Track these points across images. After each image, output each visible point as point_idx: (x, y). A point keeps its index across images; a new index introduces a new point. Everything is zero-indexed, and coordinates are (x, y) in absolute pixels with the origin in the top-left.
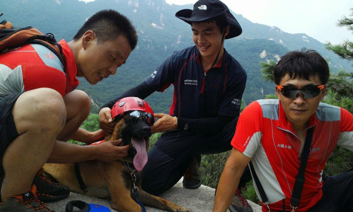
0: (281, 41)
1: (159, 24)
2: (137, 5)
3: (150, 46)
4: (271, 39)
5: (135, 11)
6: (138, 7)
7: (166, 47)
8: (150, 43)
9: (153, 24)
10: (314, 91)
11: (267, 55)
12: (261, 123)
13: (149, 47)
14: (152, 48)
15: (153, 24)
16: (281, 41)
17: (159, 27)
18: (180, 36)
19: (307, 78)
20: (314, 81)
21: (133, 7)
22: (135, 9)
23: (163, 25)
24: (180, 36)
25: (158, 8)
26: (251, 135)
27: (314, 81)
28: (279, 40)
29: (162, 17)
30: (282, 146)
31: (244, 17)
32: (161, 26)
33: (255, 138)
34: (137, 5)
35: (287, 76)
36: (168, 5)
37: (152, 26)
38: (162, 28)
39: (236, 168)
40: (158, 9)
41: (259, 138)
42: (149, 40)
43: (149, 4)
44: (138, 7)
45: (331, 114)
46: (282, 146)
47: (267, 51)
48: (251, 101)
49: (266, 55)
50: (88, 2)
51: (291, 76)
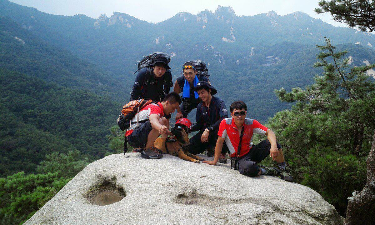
0: (369, 44)
1: (229, 38)
2: (206, 21)
3: (221, 61)
4: (358, 43)
5: (204, 27)
6: (207, 22)
7: (238, 61)
8: (221, 58)
9: (224, 39)
10: (243, 113)
11: (354, 61)
12: (227, 126)
13: (220, 62)
14: (224, 62)
15: (224, 39)
16: (369, 44)
17: (230, 41)
18: (253, 48)
19: (241, 109)
20: (243, 110)
21: (203, 24)
22: (204, 25)
23: (234, 38)
24: (253, 48)
25: (228, 22)
26: (223, 130)
27: (243, 110)
28: (367, 43)
29: (232, 30)
30: (233, 133)
31: (324, 21)
32: (232, 40)
33: (225, 132)
34: (206, 21)
35: (235, 109)
36: (238, 18)
37: (222, 41)
38: (233, 42)
39: (220, 143)
40: (228, 23)
41: (226, 132)
42: (220, 55)
43: (218, 18)
44: (207, 22)
45: (250, 122)
46: (233, 133)
47: (353, 56)
48: (228, 116)
49: (353, 61)
50: (157, 23)
51: (236, 110)
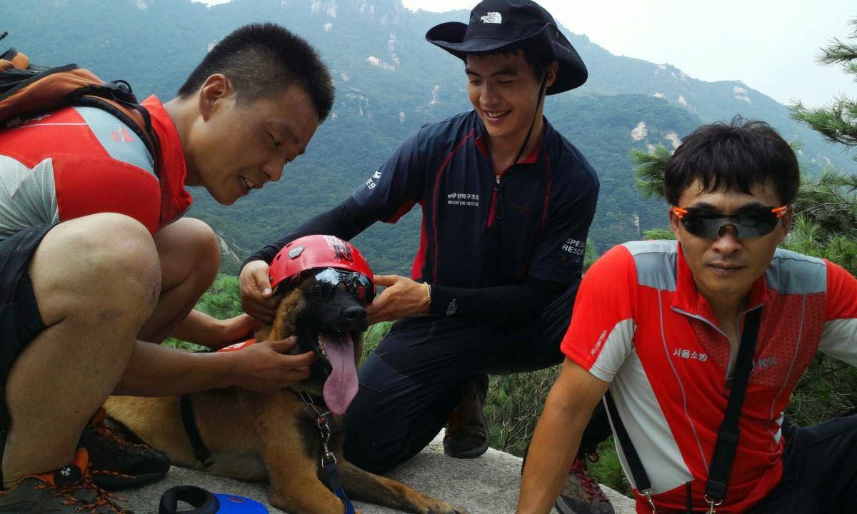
0: (682, 100)
1: (385, 58)
2: (332, 12)
3: (364, 111)
4: (658, 95)
5: (328, 26)
6: (335, 17)
7: (402, 114)
8: (363, 103)
9: (373, 59)
10: (763, 221)
11: (649, 133)
12: (634, 298)
13: (362, 114)
14: (370, 116)
15: (373, 59)
16: (682, 100)
17: (386, 66)
18: (437, 87)
19: (744, 189)
20: (762, 196)
21: (324, 18)
22: (327, 22)
23: (396, 60)
24: (437, 87)
25: (384, 20)
26: (610, 327)
27: (762, 196)
28: (677, 97)
29: (392, 41)
30: (686, 354)
31: (592, 40)
32: (391, 63)
33: (620, 334)
34: (332, 12)
35: (696, 185)
36: (408, 13)
37: (369, 64)
38: (393, 68)
39: (573, 408)
40: (383, 23)
41: (629, 336)
42: (362, 98)
43: (362, 10)
44: (335, 17)
45: (803, 277)
46: (686, 354)
47: (647, 123)
48: (609, 245)
49: (645, 134)
50: (214, 4)
51: (706, 185)
